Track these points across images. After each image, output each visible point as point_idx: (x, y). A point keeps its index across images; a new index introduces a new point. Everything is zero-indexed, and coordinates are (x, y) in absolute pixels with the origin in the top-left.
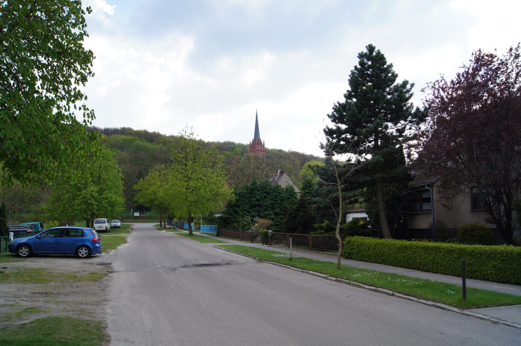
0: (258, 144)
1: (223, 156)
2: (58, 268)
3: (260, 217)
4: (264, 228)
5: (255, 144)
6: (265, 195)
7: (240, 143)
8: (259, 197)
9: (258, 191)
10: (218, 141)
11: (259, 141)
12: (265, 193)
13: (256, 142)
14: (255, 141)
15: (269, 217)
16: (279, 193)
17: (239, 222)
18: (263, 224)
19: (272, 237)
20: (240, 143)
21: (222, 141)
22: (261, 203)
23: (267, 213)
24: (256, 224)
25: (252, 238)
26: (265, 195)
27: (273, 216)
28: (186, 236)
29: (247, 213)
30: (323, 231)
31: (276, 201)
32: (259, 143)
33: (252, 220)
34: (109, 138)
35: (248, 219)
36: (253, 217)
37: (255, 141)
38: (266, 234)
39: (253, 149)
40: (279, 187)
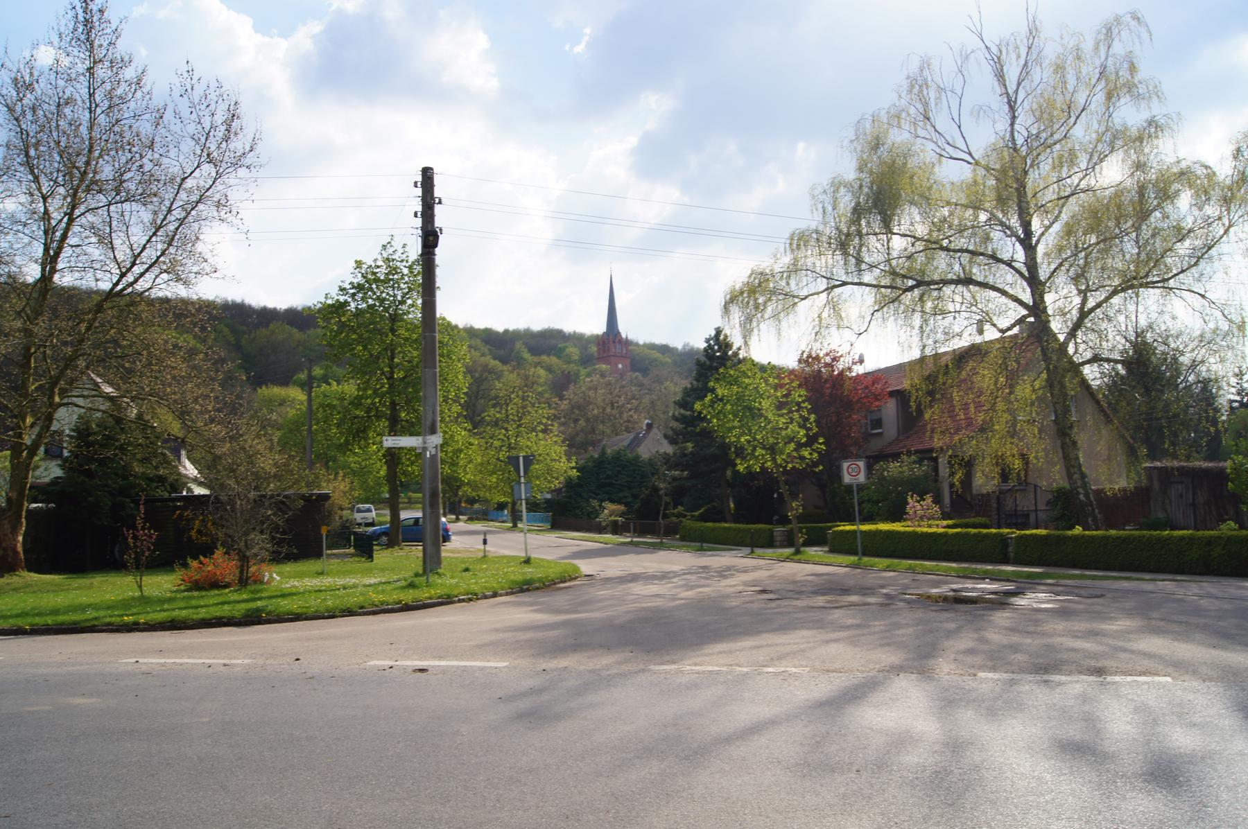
0: (614, 342)
1: (542, 372)
2: (253, 596)
3: (612, 501)
4: (616, 516)
5: (609, 343)
6: (619, 469)
7: (575, 332)
8: (610, 473)
9: (609, 464)
10: (526, 327)
11: (616, 335)
12: (618, 466)
13: (611, 337)
14: (608, 336)
15: (624, 501)
16: (639, 466)
17: (582, 509)
18: (614, 511)
19: (622, 526)
20: (575, 332)
21: (537, 327)
22: (614, 482)
23: (621, 494)
24: (606, 511)
25: (600, 530)
26: (619, 469)
27: (630, 500)
28: (509, 529)
29: (594, 496)
30: (1167, 501)
31: (635, 477)
32: (617, 341)
33: (600, 506)
34: (306, 335)
35: (595, 503)
36: (602, 501)
37: (608, 336)
38: (615, 522)
39: (604, 352)
40: (637, 457)
